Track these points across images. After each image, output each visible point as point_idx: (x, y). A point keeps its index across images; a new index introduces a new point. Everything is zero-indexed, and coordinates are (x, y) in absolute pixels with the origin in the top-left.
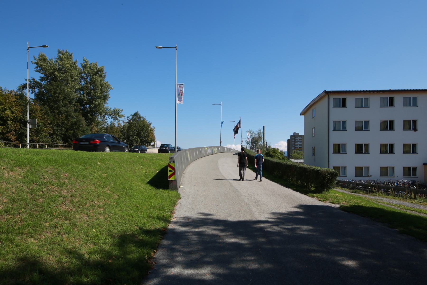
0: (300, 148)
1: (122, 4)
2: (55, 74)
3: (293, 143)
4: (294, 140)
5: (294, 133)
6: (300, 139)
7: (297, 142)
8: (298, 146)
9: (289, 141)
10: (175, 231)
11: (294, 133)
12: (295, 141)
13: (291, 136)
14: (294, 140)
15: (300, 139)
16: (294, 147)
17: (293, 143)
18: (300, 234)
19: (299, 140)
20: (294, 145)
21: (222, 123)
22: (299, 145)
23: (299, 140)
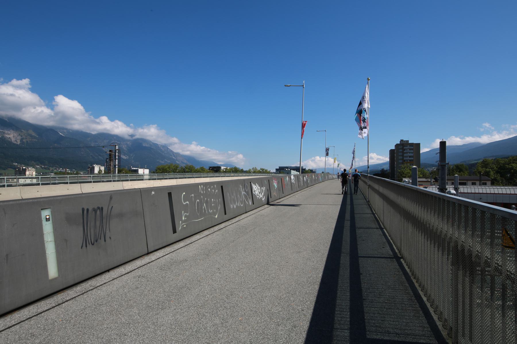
0: (410, 160)
1: (152, 10)
2: (494, 278)
3: (401, 157)
4: (401, 150)
5: (402, 141)
6: (410, 149)
7: (407, 153)
8: (408, 158)
9: (392, 152)
10: (144, 145)
11: (402, 141)
12: (403, 156)
13: (397, 146)
14: (401, 150)
15: (410, 149)
16: (403, 159)
17: (401, 157)
18: (383, 156)
19: (408, 151)
20: (401, 157)
21: (303, 126)
22: (410, 157)
23: (408, 151)
